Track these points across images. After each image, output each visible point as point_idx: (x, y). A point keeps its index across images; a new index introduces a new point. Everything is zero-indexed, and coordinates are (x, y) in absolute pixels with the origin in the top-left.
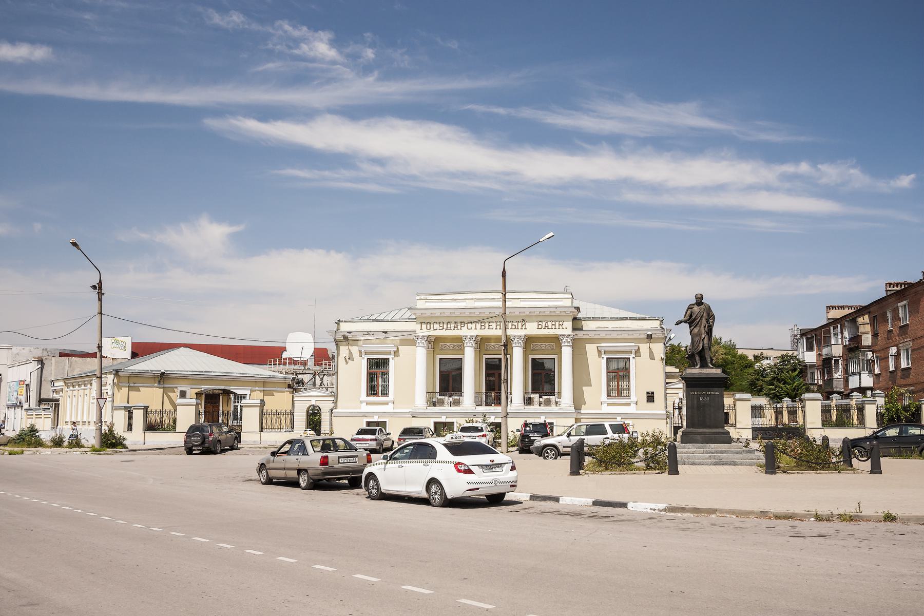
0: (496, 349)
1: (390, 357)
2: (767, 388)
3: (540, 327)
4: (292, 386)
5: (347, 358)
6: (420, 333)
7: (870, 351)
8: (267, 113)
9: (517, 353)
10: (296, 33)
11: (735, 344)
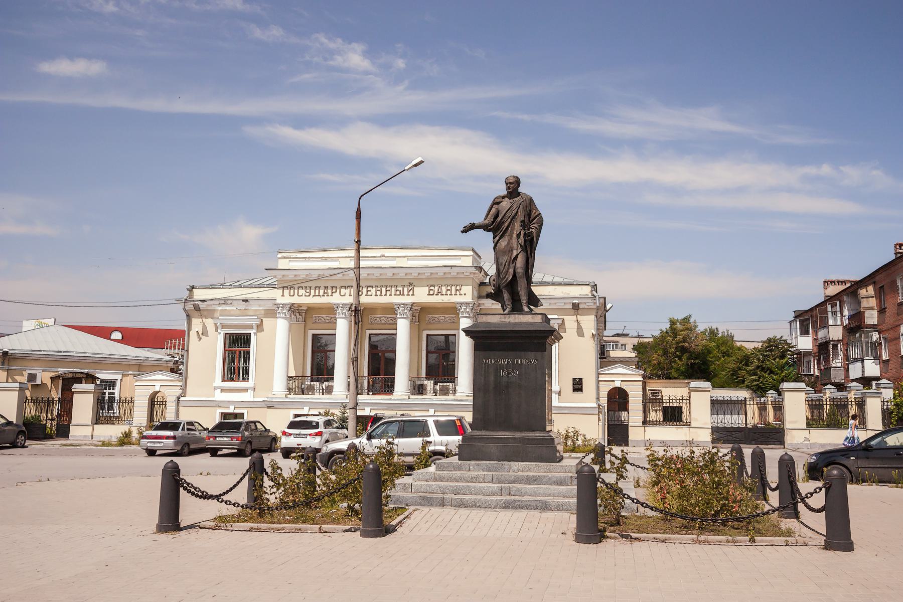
0: (383, 322)
1: (252, 332)
2: (749, 379)
3: (432, 292)
4: (175, 370)
5: (200, 333)
6: (280, 300)
7: (875, 331)
8: (302, 122)
9: (403, 329)
10: (332, 45)
11: (732, 334)
